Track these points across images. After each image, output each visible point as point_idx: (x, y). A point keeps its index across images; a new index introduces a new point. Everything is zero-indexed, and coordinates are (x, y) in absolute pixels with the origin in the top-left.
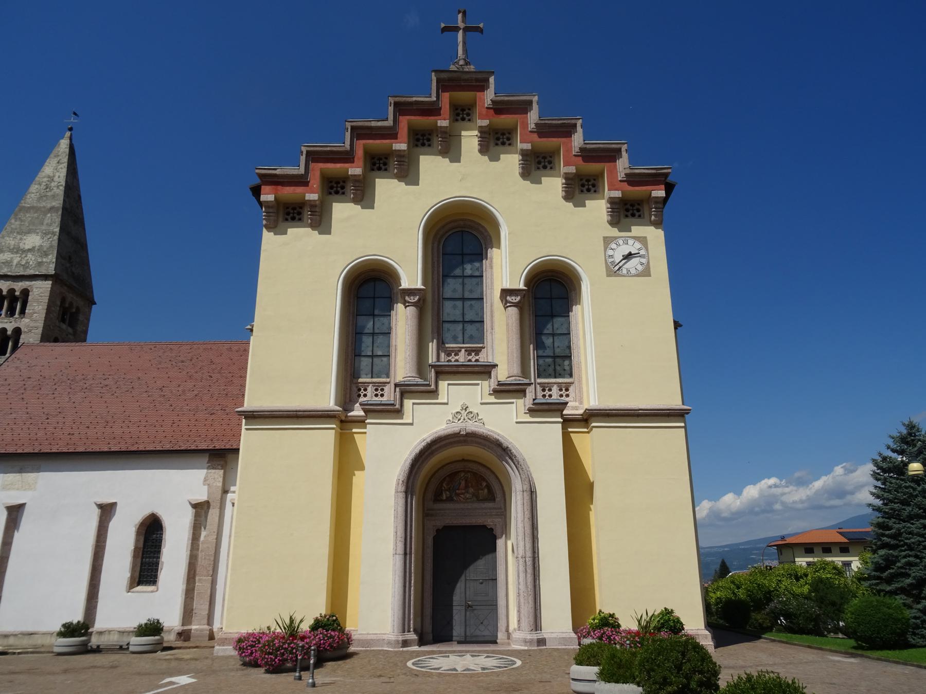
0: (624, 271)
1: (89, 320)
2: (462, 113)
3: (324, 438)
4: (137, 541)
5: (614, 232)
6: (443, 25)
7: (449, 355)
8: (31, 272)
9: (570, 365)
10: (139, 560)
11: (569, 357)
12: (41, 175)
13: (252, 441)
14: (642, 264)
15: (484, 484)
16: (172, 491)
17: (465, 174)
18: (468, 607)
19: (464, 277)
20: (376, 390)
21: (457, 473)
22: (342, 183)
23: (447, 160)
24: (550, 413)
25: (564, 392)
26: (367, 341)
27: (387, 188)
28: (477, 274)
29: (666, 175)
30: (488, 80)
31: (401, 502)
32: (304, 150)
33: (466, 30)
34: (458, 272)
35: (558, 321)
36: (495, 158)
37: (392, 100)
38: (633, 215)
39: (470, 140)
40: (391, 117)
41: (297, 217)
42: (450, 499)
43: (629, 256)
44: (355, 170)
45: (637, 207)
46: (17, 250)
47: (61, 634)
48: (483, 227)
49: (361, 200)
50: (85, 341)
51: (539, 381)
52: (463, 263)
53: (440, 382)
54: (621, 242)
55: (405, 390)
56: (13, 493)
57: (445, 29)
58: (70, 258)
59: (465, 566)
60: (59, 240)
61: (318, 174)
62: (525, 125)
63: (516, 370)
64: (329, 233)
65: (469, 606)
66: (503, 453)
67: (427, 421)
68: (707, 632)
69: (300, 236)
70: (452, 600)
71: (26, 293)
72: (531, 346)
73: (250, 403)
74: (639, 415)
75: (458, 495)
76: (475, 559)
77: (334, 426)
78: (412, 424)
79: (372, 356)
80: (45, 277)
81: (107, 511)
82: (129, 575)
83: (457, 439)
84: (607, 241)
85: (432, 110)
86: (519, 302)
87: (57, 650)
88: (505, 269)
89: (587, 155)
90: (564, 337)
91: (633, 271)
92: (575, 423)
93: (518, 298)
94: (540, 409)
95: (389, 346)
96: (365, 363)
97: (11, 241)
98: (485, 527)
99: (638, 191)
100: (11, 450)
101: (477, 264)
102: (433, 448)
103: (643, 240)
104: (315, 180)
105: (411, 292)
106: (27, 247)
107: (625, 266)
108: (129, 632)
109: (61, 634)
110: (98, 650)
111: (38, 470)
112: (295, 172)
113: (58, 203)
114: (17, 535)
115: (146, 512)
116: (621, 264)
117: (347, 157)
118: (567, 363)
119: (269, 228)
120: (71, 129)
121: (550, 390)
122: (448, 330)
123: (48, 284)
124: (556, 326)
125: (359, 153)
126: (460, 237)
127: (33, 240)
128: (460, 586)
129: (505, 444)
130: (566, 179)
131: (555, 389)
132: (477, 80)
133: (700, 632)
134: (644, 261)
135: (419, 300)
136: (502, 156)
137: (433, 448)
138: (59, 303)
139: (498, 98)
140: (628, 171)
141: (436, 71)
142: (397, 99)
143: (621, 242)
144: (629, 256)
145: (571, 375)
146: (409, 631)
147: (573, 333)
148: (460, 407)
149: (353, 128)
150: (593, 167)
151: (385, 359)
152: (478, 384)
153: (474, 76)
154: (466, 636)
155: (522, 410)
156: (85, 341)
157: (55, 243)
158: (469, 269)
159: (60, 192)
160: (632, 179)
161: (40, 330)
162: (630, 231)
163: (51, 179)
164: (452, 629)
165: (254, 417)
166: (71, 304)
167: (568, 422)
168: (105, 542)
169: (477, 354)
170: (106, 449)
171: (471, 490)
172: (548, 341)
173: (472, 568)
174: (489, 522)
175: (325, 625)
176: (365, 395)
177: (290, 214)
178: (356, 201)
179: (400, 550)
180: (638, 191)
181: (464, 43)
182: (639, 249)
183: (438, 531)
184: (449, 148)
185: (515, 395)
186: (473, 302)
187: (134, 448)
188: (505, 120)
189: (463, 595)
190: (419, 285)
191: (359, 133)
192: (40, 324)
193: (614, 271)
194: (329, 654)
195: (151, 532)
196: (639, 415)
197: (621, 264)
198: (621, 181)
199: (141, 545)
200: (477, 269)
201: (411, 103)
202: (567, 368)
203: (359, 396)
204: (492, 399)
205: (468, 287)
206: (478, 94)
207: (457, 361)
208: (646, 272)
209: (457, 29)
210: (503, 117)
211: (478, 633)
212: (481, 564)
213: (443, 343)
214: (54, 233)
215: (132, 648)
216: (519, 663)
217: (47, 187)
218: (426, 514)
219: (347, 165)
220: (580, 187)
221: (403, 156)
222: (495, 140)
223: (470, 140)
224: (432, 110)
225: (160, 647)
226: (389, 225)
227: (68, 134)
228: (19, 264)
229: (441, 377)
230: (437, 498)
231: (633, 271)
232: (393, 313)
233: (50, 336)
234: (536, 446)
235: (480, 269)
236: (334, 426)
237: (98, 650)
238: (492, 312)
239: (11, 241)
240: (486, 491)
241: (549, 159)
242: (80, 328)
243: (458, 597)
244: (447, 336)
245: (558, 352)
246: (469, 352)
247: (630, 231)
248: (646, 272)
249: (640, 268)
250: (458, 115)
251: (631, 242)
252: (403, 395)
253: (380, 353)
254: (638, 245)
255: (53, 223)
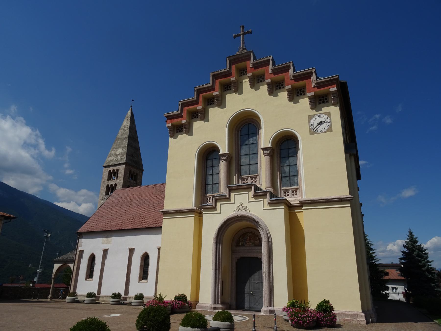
0: (319, 131)
1: (142, 178)
2: (242, 72)
3: (190, 220)
4: (141, 263)
5: (314, 112)
6: (234, 35)
7: (244, 180)
8: (119, 163)
9: (297, 180)
10: (142, 270)
11: (297, 175)
12: (123, 125)
13: (167, 223)
14: (328, 126)
15: (258, 238)
16: (144, 243)
17: (249, 98)
18: (251, 294)
19: (249, 144)
20: (293, 192)
21: (246, 233)
22: (303, 90)
23: (237, 94)
24: (279, 204)
25: (295, 193)
26: (210, 178)
27: (214, 112)
28: (255, 142)
29: (337, 79)
30: (250, 55)
31: (214, 247)
32: (180, 103)
33: (244, 34)
34: (247, 142)
35: (291, 159)
36: (257, 89)
37: (211, 74)
38: (323, 102)
39: (246, 83)
40: (211, 82)
41: (325, 101)
42: (243, 245)
43: (321, 123)
44: (199, 107)
45: (325, 97)
46: (116, 155)
47: (112, 297)
48: (256, 120)
49: (293, 100)
50: (141, 185)
51: (282, 188)
52: (249, 138)
53: (232, 194)
54: (317, 117)
55: (218, 199)
56: (105, 245)
57: (235, 37)
58: (132, 155)
59: (250, 276)
60: (127, 149)
61: (186, 111)
62: (268, 71)
63: (269, 185)
64: (192, 135)
65: (252, 294)
66: (256, 224)
67: (226, 211)
68: (363, 314)
69: (182, 138)
70: (244, 291)
71: (118, 170)
72: (278, 173)
73: (168, 207)
74: (326, 202)
75: (246, 243)
76: (254, 273)
77: (283, 207)
78: (220, 213)
79: (212, 184)
80: (122, 164)
81: (132, 251)
82: (139, 276)
83: (237, 219)
84: (310, 117)
85: (228, 74)
86: (270, 153)
87: (111, 303)
88: (265, 139)
89: (297, 78)
90: (295, 166)
91: (323, 130)
92: (298, 208)
93: (269, 151)
94: (275, 202)
95: (219, 179)
96: (210, 187)
97: (113, 152)
98: (257, 258)
99: (322, 90)
100: (104, 229)
101: (255, 138)
102: (228, 223)
103: (328, 114)
104: (185, 114)
105: (223, 155)
106: (118, 153)
107: (320, 128)
108: (84, 296)
109: (112, 297)
110: (78, 302)
111: (111, 236)
112: (177, 113)
113: (127, 135)
114: (106, 260)
115: (144, 252)
116: (317, 128)
117: (196, 102)
118: (296, 178)
119: (171, 137)
120: (131, 107)
121: (288, 192)
122: (243, 169)
123: (123, 166)
124: (290, 161)
125: (201, 99)
126: (245, 127)
127: (120, 151)
128: (248, 285)
129: (257, 220)
130: (288, 92)
131: (290, 191)
132: (246, 56)
133: (358, 313)
134: (329, 124)
135: (227, 158)
136: (260, 87)
137: (228, 223)
138: (129, 173)
139: (255, 62)
140: (316, 82)
141: (228, 57)
142: (214, 73)
143: (317, 117)
144: (321, 123)
145: (298, 184)
146: (218, 303)
147: (298, 164)
148: (242, 204)
149: (197, 90)
150: (301, 83)
151: (217, 185)
152: (247, 193)
153: (244, 55)
154: (250, 308)
155: (266, 203)
156: (141, 185)
157: (126, 151)
158: (251, 140)
159: (127, 131)
160: (319, 85)
161: (122, 184)
162: (322, 110)
163: (125, 127)
164: (244, 304)
165: (166, 213)
166: (134, 173)
167: (291, 209)
168: (131, 263)
169: (255, 179)
170: (131, 228)
171: (252, 241)
172: (287, 169)
173: (253, 276)
174: (255, 255)
175: (178, 298)
176: (210, 201)
177: (178, 129)
178: (202, 120)
179: (214, 268)
180: (322, 90)
181: (243, 40)
182: (326, 119)
183: (238, 259)
184: (237, 88)
185: (263, 197)
186: (253, 155)
187: (139, 227)
188: (260, 71)
189: (249, 289)
190: (227, 152)
191: (200, 91)
192: (122, 182)
193: (313, 131)
194: (178, 310)
195: (146, 258)
196: (326, 202)
197: (317, 128)
198: (313, 87)
199: (143, 264)
200: (255, 140)
201: (220, 74)
202: (296, 181)
203: (207, 202)
204: (253, 200)
205: (251, 149)
206: (247, 62)
207: (247, 183)
208: (330, 129)
209: (240, 35)
210: (258, 70)
211: (255, 306)
212: (256, 274)
213: (241, 175)
214: (125, 147)
215: (133, 304)
216: (248, 318)
217: (124, 130)
218: (233, 252)
219: (196, 106)
220: (295, 94)
221: (218, 97)
222: (256, 81)
223: (246, 83)
224: (228, 74)
225: (142, 304)
226: (214, 129)
227: (131, 108)
228: (115, 160)
229: (232, 191)
230: (238, 245)
231: (323, 130)
232: (220, 164)
233: (126, 185)
234: (272, 221)
235: (256, 140)
236: (283, 207)
237: (78, 302)
238: (261, 159)
239: (113, 152)
240: (258, 241)
241: (282, 83)
242: (138, 181)
243: (247, 290)
244: (242, 172)
245: (292, 174)
246: (252, 178)
247: (322, 110)
248: (330, 129)
249: (327, 128)
250: (241, 73)
251: (322, 116)
252: (216, 201)
253: (215, 183)
254: (326, 117)
255: (125, 143)
